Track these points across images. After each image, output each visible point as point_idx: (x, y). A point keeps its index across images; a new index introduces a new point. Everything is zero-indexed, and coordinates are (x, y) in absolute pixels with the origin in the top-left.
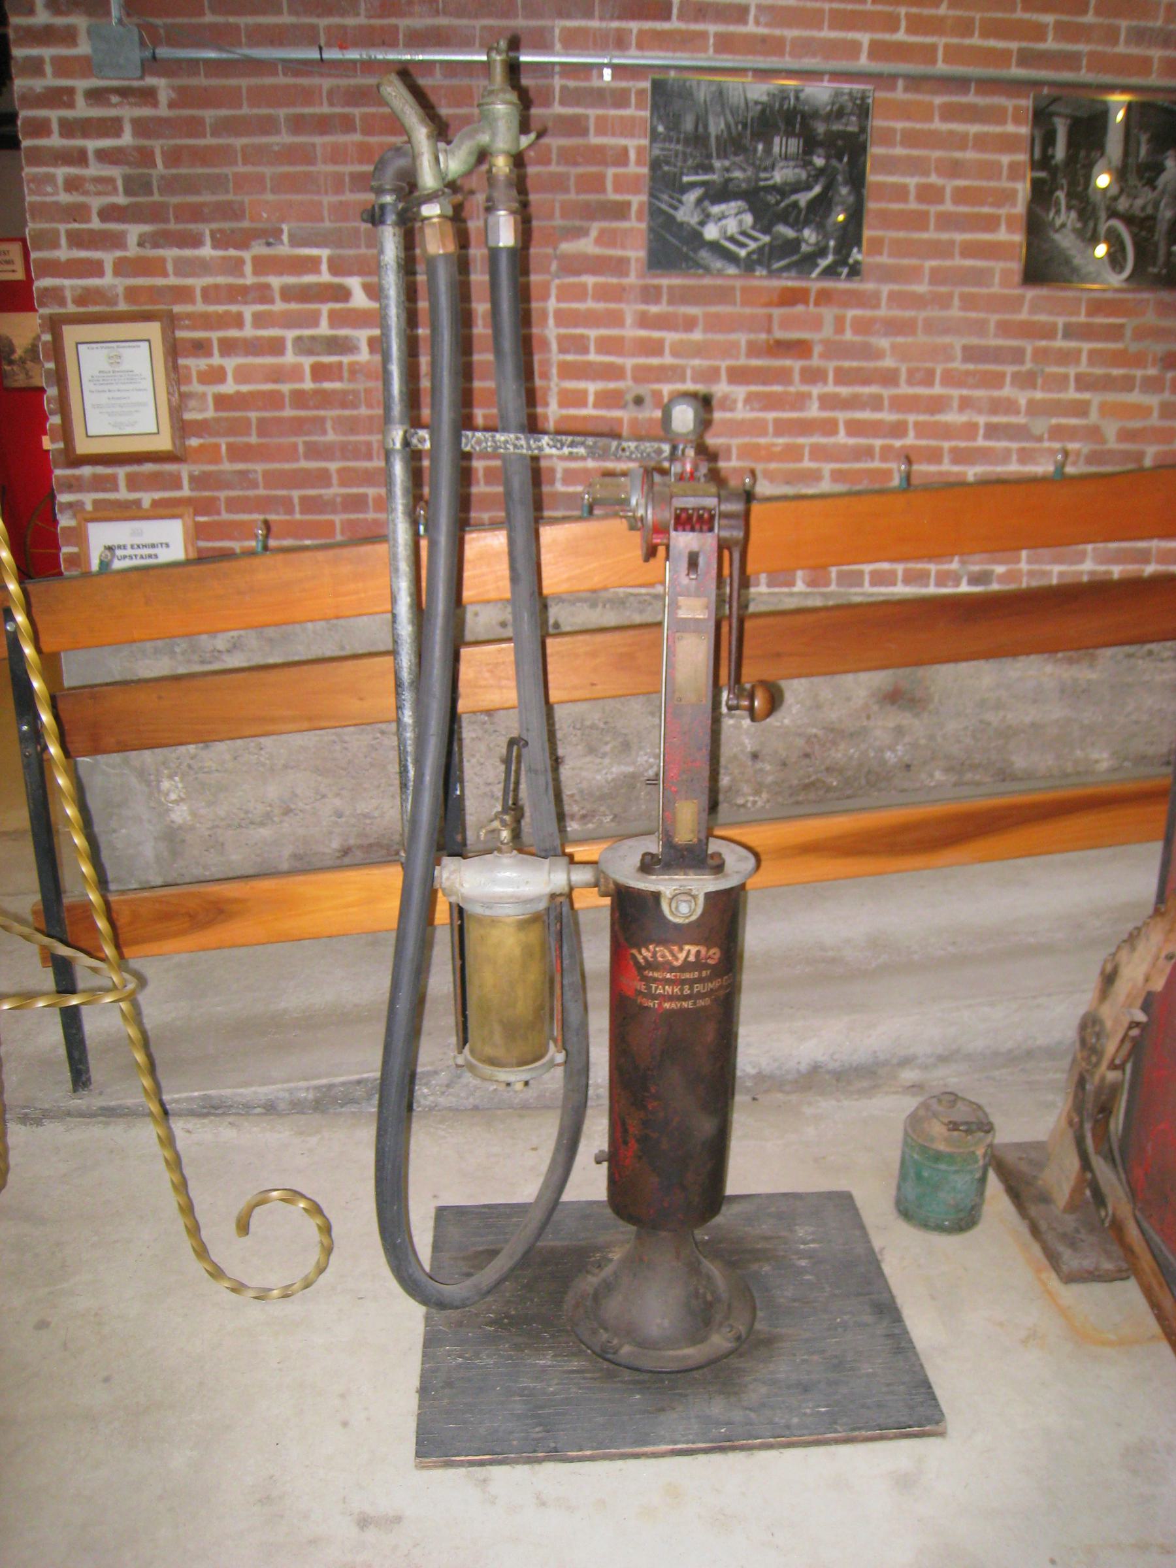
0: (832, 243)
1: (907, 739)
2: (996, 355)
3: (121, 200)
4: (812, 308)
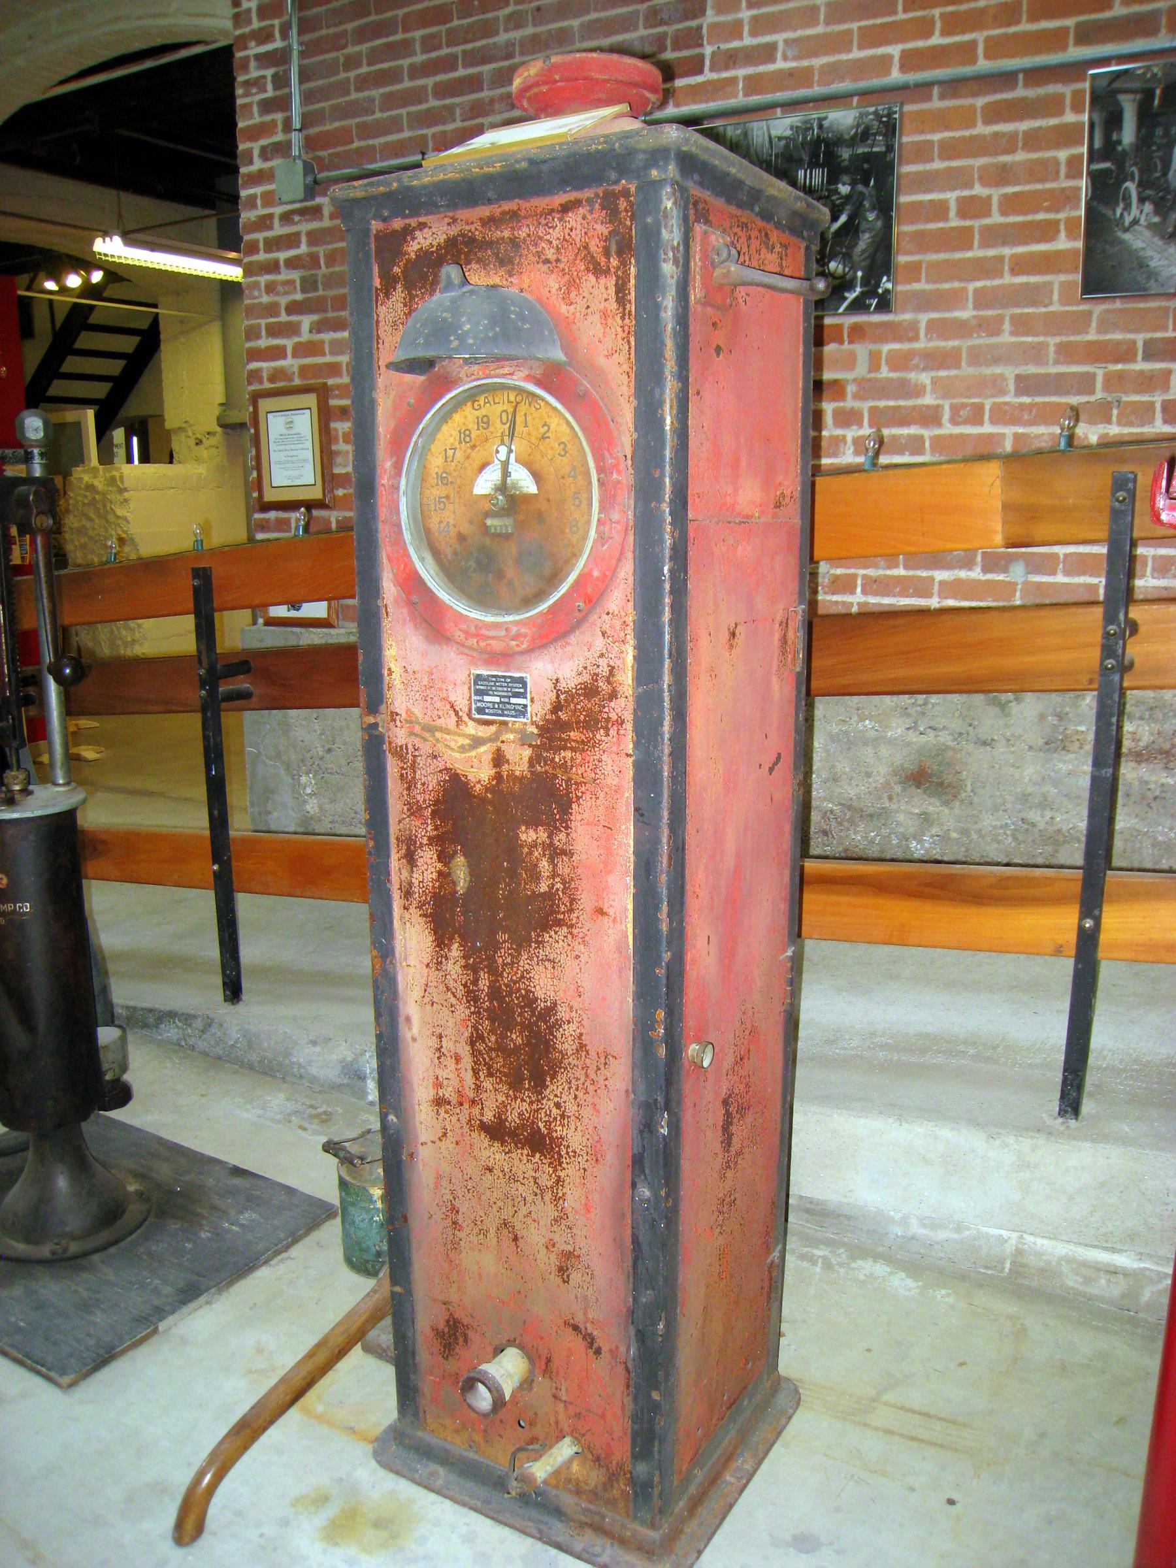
0: (860, 274)
1: (935, 830)
2: (1058, 384)
3: (299, 297)
4: (846, 346)
